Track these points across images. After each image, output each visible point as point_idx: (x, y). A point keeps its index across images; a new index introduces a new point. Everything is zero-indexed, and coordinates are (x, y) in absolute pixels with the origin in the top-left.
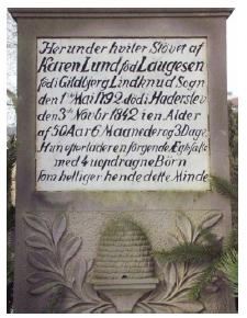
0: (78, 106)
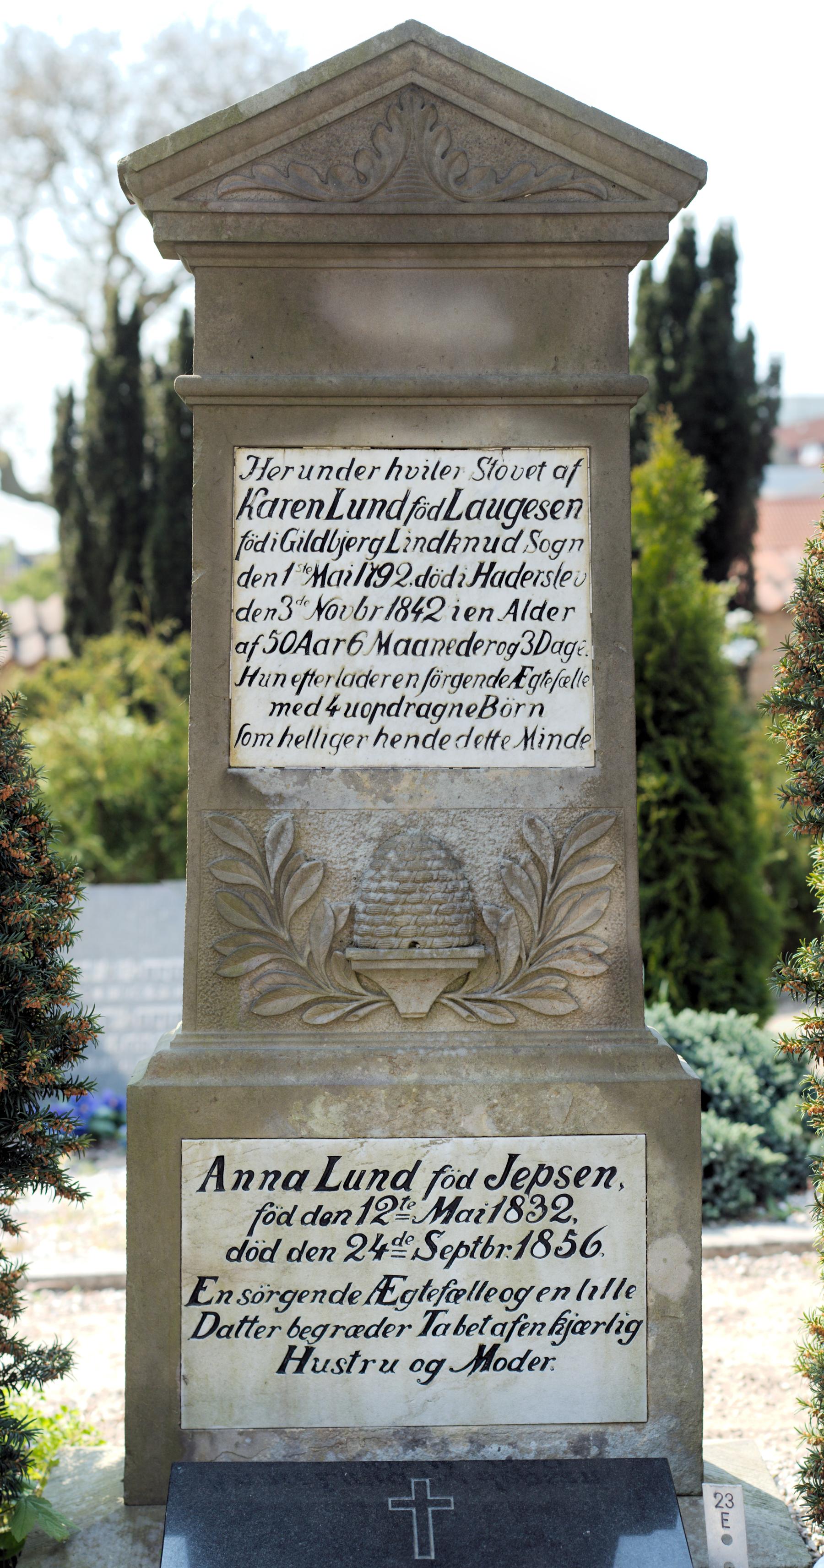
0: (318, 591)
